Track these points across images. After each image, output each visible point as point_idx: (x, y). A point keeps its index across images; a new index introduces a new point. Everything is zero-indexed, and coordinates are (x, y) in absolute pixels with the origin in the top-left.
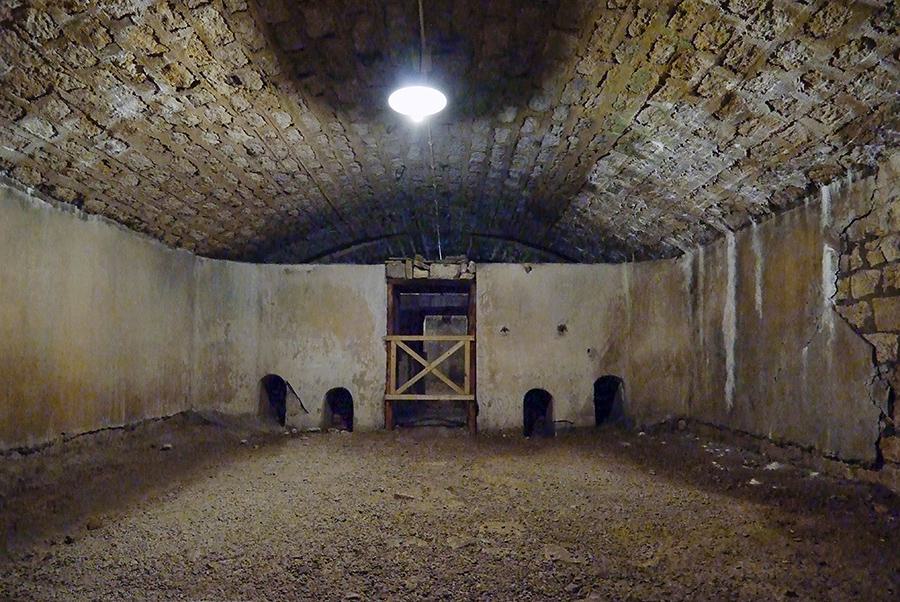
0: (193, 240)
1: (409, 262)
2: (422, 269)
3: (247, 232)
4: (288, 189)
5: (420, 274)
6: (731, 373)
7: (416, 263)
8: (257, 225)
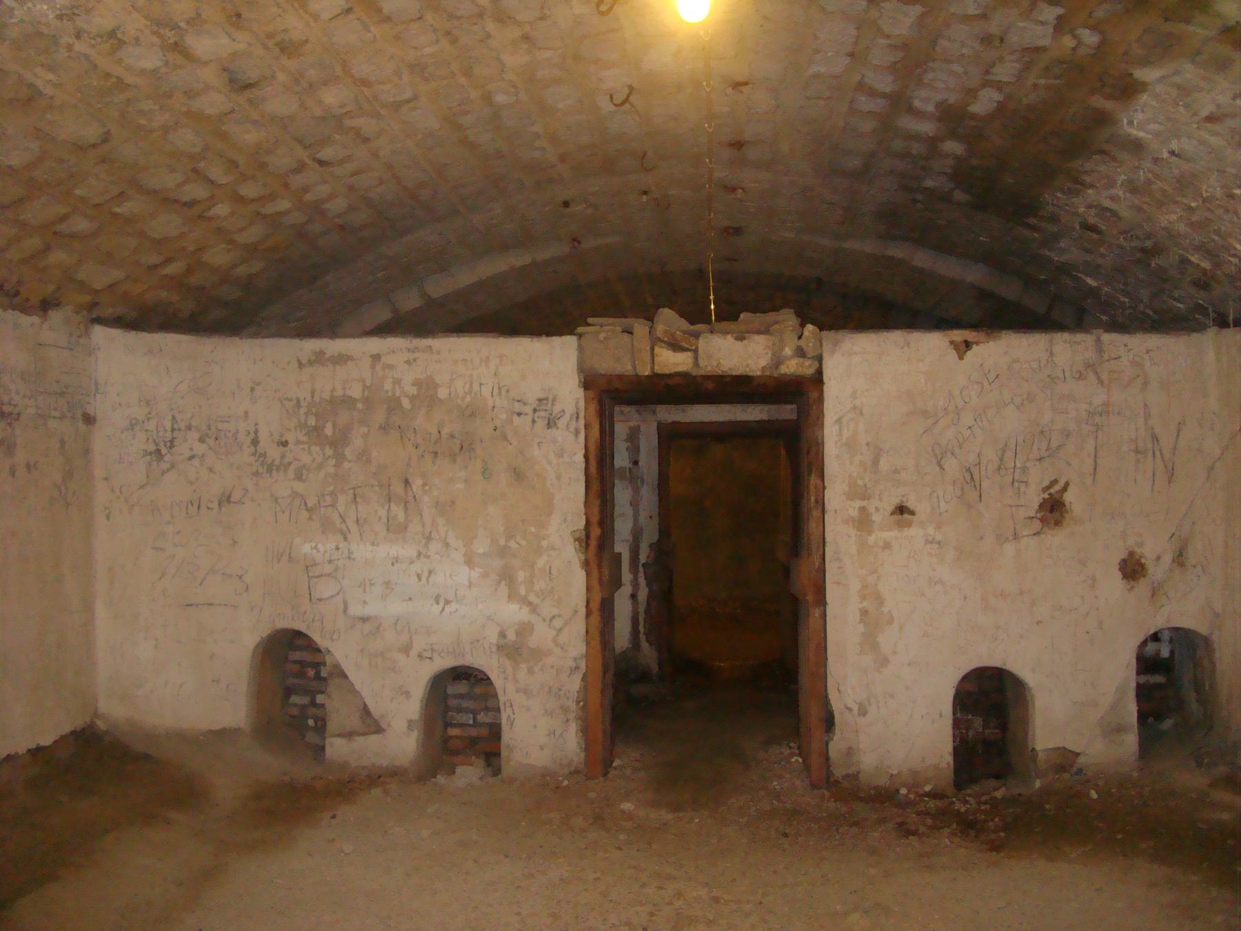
0: (82, 286)
1: (640, 327)
2: (675, 347)
3: (219, 256)
4: (326, 153)
5: (673, 361)
6: (608, 430)
7: (660, 328)
8: (245, 238)
